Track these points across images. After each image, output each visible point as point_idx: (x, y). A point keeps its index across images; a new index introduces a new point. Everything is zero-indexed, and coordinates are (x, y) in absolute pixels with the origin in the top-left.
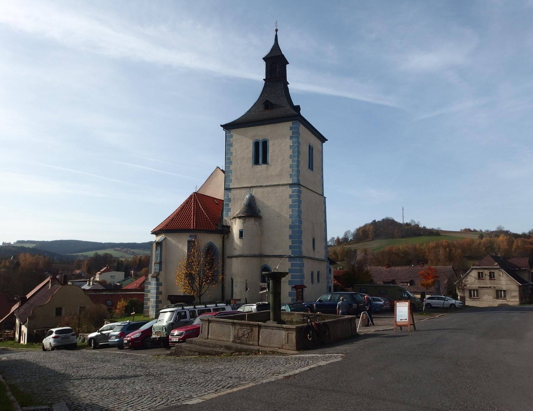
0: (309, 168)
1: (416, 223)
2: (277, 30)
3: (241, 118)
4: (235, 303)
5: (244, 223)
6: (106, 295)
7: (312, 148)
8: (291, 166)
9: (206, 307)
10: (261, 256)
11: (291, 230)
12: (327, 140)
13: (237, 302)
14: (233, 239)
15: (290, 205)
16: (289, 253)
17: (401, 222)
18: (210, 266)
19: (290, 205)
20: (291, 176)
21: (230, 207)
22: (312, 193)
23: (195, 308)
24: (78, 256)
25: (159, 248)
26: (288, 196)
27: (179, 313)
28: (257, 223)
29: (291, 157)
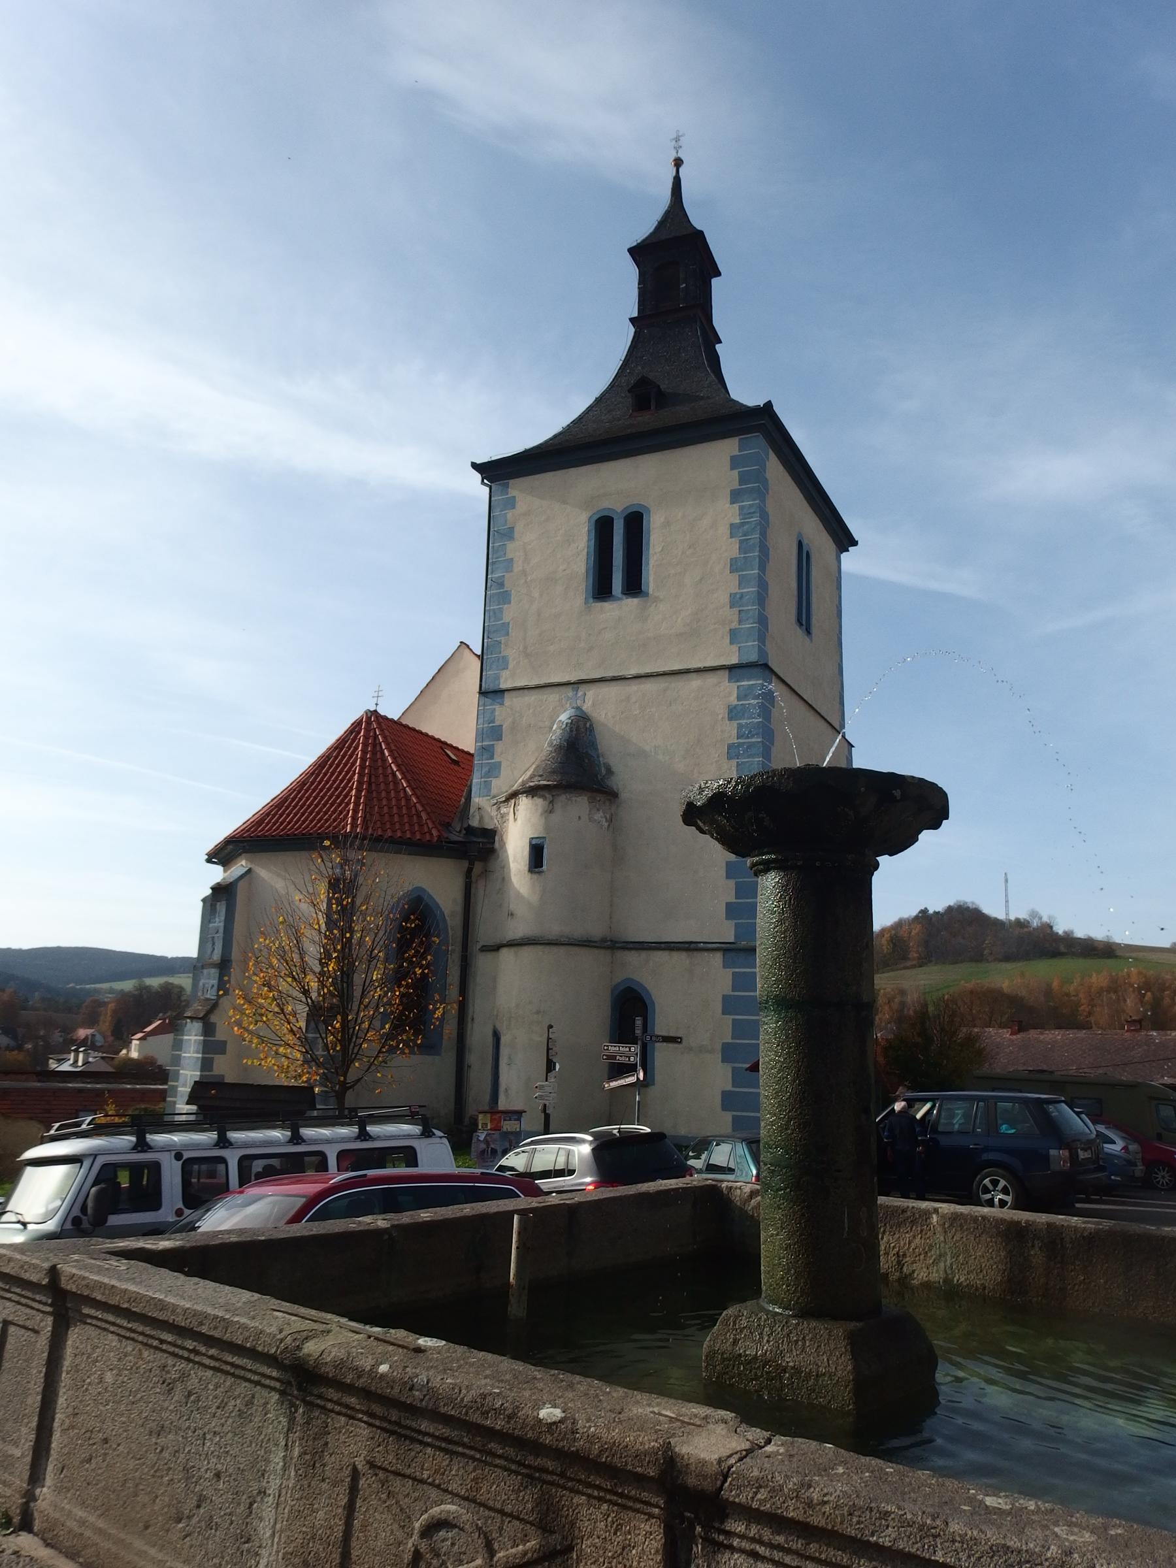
0: (799, 621)
1: (1045, 919)
2: (678, 163)
3: (546, 442)
4: (497, 1128)
5: (549, 811)
6: (80, 1090)
8: (735, 601)
9: (296, 1139)
10: (613, 945)
13: (508, 1126)
14: (505, 880)
15: (730, 747)
17: (1001, 916)
18: (414, 979)
19: (730, 747)
20: (734, 635)
21: (496, 759)
22: (811, 716)
23: (223, 1142)
24: (96, 991)
25: (221, 908)
26: (722, 712)
27: (106, 1175)
28: (598, 816)
29: (735, 566)
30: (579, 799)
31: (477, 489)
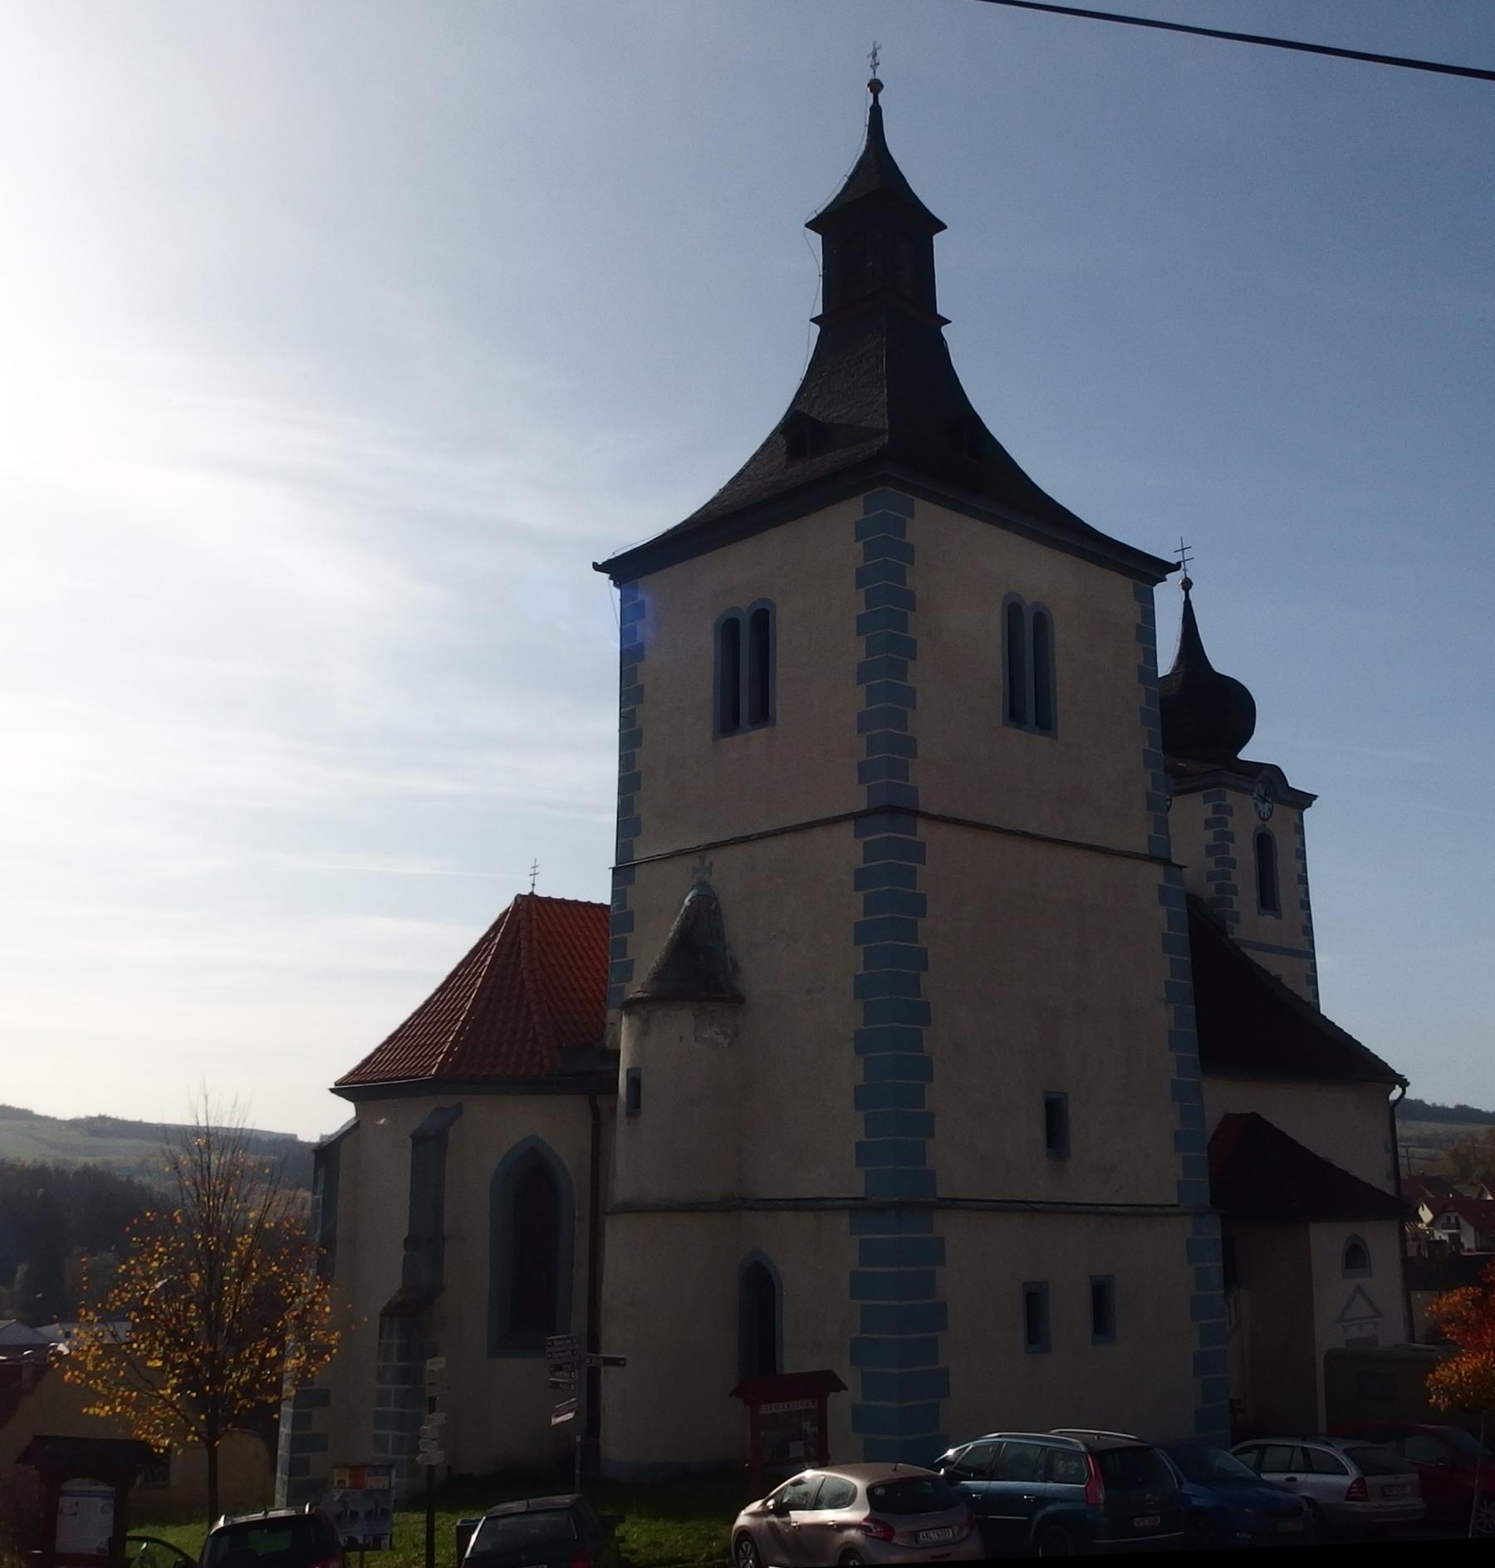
2: (876, 86)
10: (737, 1204)
12: (1315, 797)
19: (857, 925)
31: (608, 594)
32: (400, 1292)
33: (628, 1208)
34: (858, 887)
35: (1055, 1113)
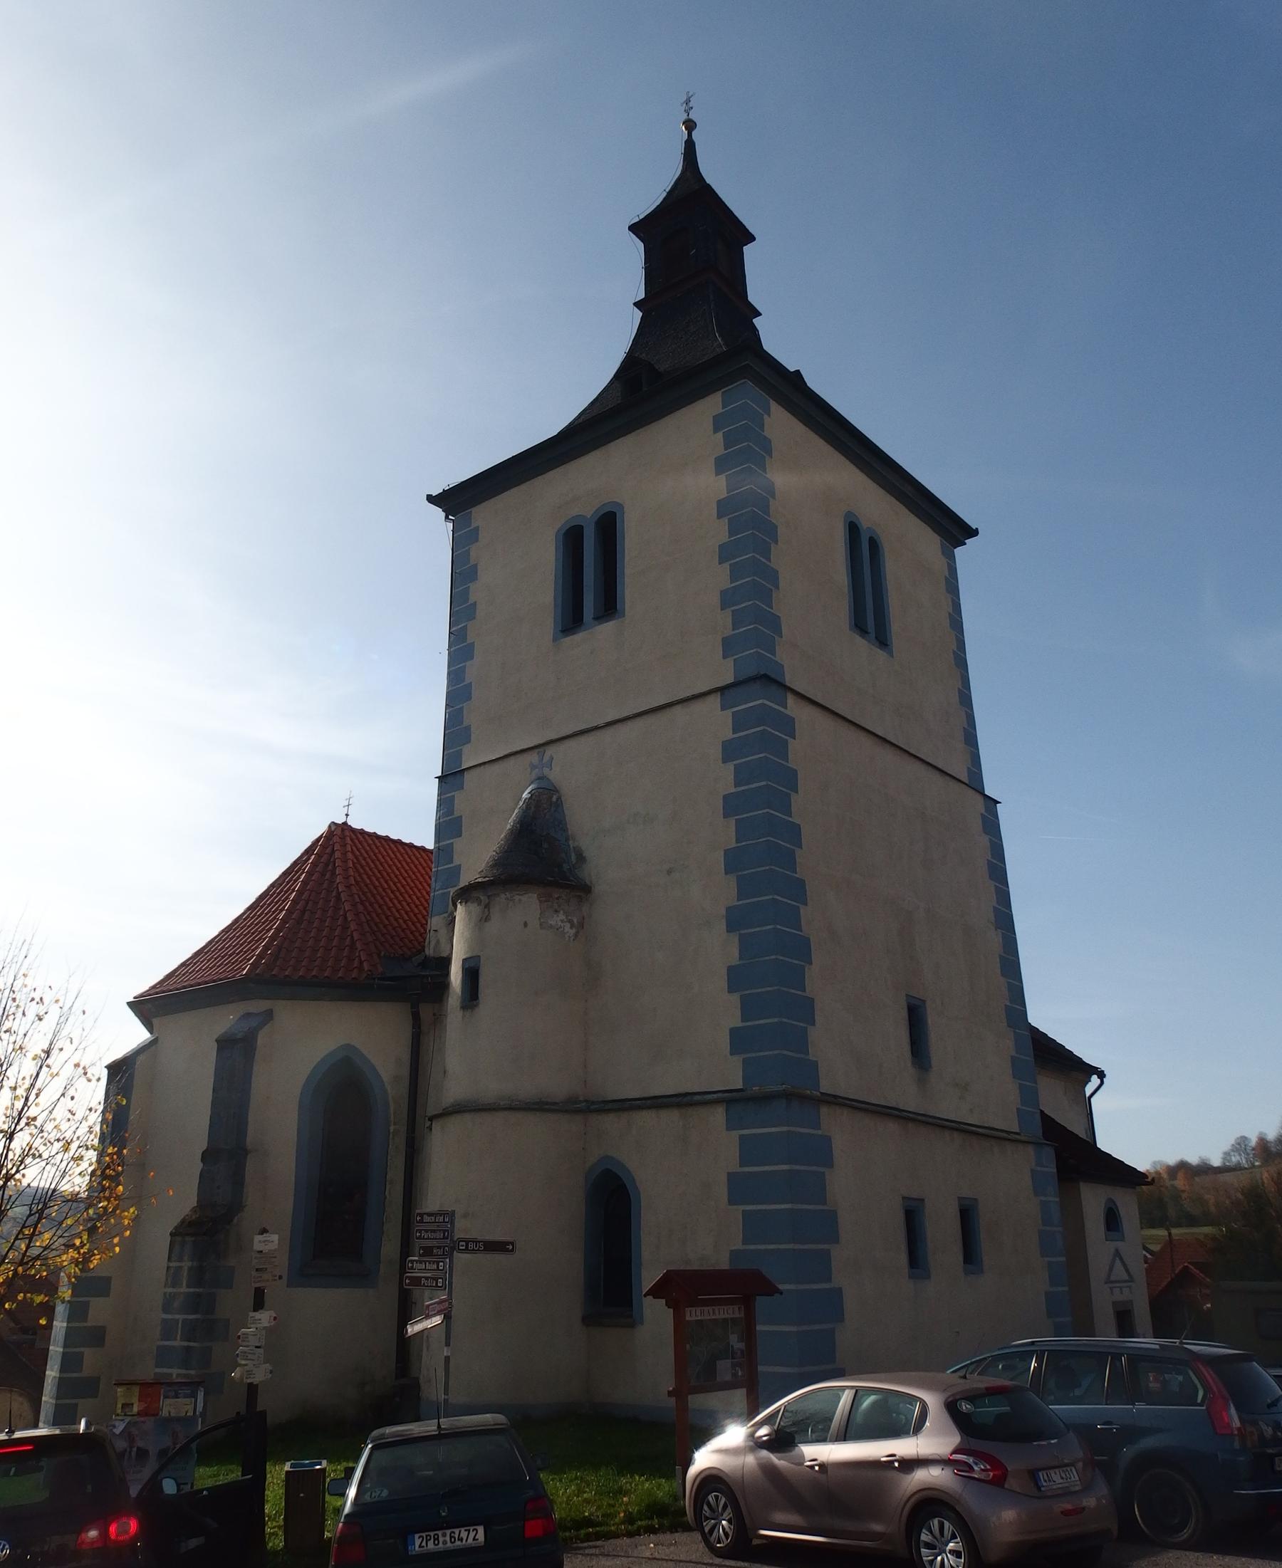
0: (859, 626)
2: (690, 125)
7: (874, 544)
10: (587, 1107)
11: (735, 938)
12: (974, 533)
16: (731, 1076)
22: (887, 757)
26: (716, 752)
28: (557, 919)
30: (524, 898)
31: (438, 527)
32: (194, 1210)
33: (459, 1109)
34: (726, 760)
35: (915, 1016)
